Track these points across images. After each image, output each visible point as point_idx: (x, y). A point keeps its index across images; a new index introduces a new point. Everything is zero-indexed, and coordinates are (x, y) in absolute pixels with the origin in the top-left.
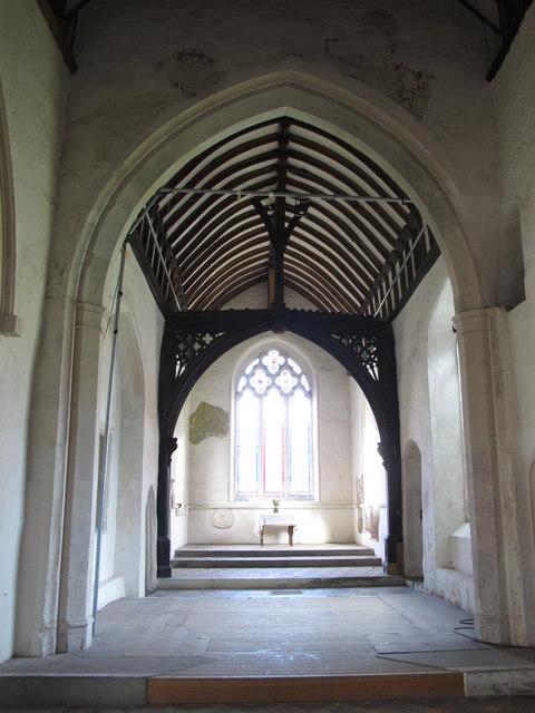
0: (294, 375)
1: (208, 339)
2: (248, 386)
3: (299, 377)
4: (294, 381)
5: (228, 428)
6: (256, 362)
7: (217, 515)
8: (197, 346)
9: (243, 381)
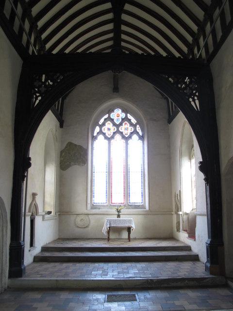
0: (131, 124)
2: (101, 132)
3: (134, 126)
4: (131, 129)
6: (106, 116)
7: (79, 219)
9: (97, 129)
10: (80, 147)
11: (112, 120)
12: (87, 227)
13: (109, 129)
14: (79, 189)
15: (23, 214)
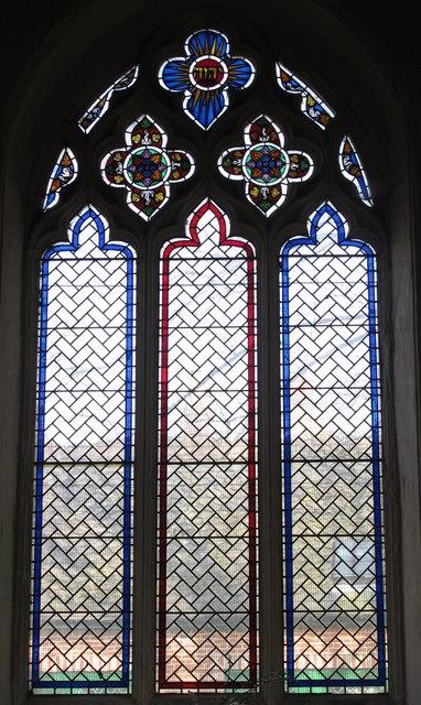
0: (301, 132)
11: (166, 108)
13: (146, 168)
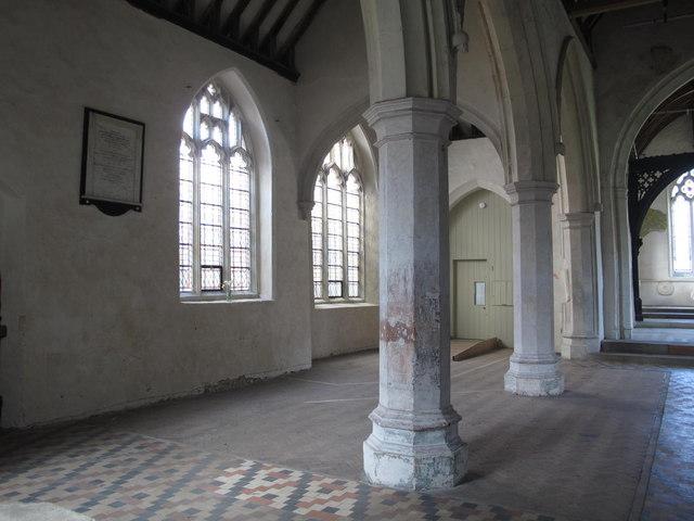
1: (658, 174)
2: (680, 193)
5: (667, 226)
6: (685, 175)
7: (661, 287)
8: (651, 180)
9: (675, 190)
10: (658, 212)
12: (594, 436)
14: (660, 254)
15: (504, 77)
